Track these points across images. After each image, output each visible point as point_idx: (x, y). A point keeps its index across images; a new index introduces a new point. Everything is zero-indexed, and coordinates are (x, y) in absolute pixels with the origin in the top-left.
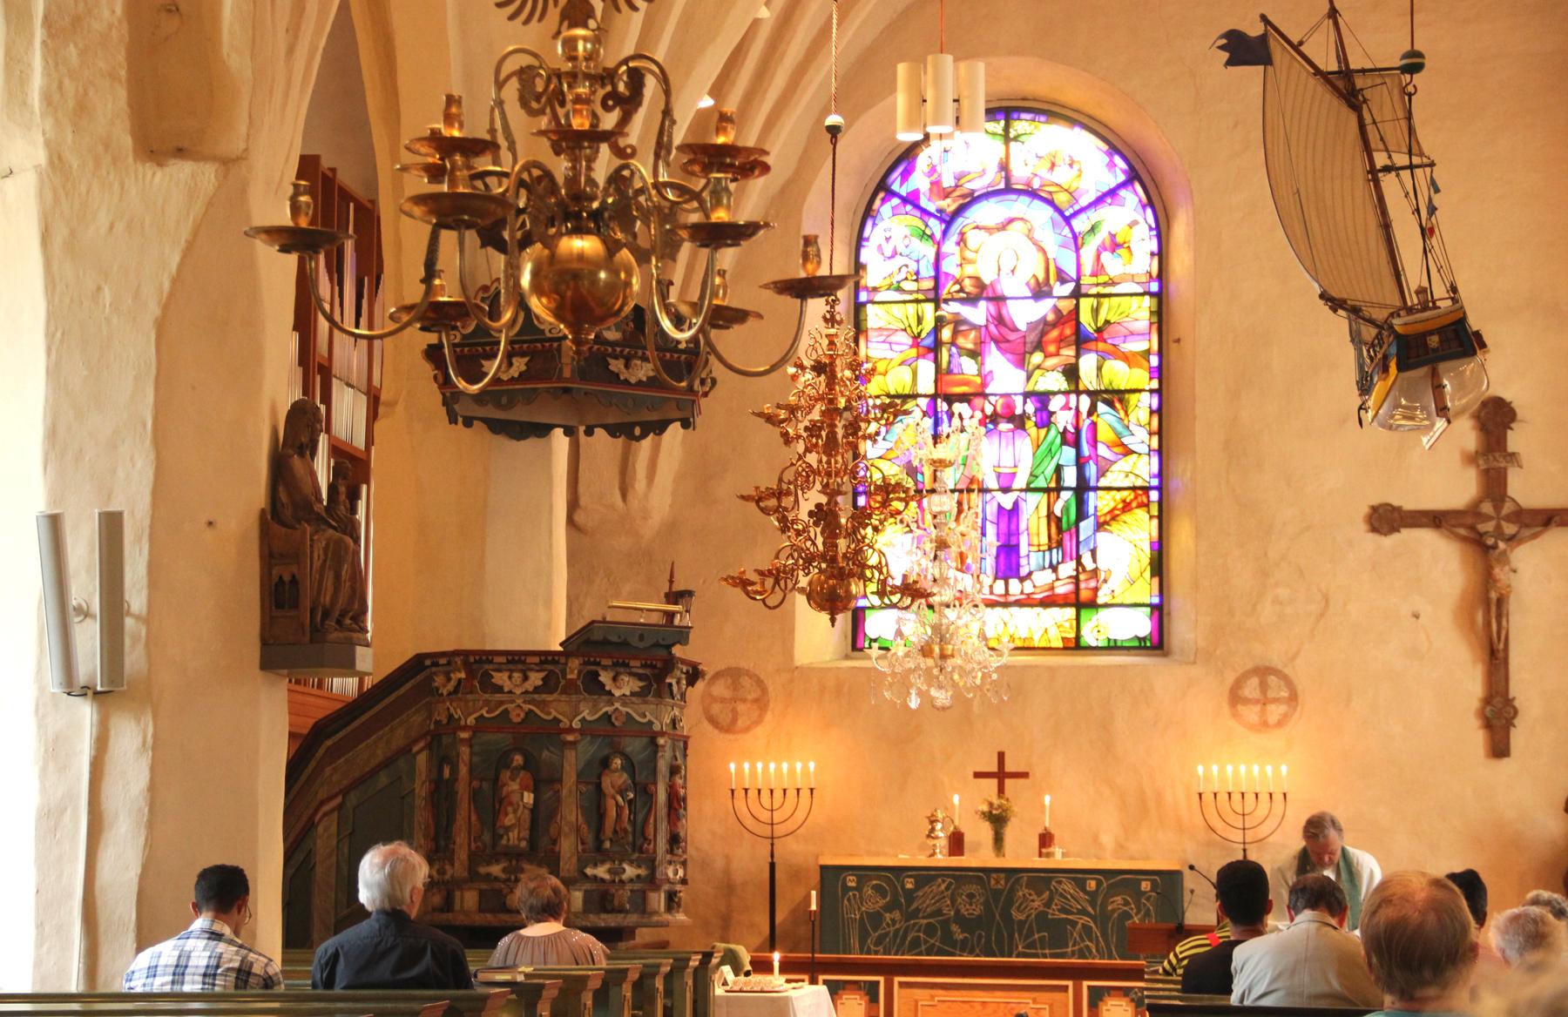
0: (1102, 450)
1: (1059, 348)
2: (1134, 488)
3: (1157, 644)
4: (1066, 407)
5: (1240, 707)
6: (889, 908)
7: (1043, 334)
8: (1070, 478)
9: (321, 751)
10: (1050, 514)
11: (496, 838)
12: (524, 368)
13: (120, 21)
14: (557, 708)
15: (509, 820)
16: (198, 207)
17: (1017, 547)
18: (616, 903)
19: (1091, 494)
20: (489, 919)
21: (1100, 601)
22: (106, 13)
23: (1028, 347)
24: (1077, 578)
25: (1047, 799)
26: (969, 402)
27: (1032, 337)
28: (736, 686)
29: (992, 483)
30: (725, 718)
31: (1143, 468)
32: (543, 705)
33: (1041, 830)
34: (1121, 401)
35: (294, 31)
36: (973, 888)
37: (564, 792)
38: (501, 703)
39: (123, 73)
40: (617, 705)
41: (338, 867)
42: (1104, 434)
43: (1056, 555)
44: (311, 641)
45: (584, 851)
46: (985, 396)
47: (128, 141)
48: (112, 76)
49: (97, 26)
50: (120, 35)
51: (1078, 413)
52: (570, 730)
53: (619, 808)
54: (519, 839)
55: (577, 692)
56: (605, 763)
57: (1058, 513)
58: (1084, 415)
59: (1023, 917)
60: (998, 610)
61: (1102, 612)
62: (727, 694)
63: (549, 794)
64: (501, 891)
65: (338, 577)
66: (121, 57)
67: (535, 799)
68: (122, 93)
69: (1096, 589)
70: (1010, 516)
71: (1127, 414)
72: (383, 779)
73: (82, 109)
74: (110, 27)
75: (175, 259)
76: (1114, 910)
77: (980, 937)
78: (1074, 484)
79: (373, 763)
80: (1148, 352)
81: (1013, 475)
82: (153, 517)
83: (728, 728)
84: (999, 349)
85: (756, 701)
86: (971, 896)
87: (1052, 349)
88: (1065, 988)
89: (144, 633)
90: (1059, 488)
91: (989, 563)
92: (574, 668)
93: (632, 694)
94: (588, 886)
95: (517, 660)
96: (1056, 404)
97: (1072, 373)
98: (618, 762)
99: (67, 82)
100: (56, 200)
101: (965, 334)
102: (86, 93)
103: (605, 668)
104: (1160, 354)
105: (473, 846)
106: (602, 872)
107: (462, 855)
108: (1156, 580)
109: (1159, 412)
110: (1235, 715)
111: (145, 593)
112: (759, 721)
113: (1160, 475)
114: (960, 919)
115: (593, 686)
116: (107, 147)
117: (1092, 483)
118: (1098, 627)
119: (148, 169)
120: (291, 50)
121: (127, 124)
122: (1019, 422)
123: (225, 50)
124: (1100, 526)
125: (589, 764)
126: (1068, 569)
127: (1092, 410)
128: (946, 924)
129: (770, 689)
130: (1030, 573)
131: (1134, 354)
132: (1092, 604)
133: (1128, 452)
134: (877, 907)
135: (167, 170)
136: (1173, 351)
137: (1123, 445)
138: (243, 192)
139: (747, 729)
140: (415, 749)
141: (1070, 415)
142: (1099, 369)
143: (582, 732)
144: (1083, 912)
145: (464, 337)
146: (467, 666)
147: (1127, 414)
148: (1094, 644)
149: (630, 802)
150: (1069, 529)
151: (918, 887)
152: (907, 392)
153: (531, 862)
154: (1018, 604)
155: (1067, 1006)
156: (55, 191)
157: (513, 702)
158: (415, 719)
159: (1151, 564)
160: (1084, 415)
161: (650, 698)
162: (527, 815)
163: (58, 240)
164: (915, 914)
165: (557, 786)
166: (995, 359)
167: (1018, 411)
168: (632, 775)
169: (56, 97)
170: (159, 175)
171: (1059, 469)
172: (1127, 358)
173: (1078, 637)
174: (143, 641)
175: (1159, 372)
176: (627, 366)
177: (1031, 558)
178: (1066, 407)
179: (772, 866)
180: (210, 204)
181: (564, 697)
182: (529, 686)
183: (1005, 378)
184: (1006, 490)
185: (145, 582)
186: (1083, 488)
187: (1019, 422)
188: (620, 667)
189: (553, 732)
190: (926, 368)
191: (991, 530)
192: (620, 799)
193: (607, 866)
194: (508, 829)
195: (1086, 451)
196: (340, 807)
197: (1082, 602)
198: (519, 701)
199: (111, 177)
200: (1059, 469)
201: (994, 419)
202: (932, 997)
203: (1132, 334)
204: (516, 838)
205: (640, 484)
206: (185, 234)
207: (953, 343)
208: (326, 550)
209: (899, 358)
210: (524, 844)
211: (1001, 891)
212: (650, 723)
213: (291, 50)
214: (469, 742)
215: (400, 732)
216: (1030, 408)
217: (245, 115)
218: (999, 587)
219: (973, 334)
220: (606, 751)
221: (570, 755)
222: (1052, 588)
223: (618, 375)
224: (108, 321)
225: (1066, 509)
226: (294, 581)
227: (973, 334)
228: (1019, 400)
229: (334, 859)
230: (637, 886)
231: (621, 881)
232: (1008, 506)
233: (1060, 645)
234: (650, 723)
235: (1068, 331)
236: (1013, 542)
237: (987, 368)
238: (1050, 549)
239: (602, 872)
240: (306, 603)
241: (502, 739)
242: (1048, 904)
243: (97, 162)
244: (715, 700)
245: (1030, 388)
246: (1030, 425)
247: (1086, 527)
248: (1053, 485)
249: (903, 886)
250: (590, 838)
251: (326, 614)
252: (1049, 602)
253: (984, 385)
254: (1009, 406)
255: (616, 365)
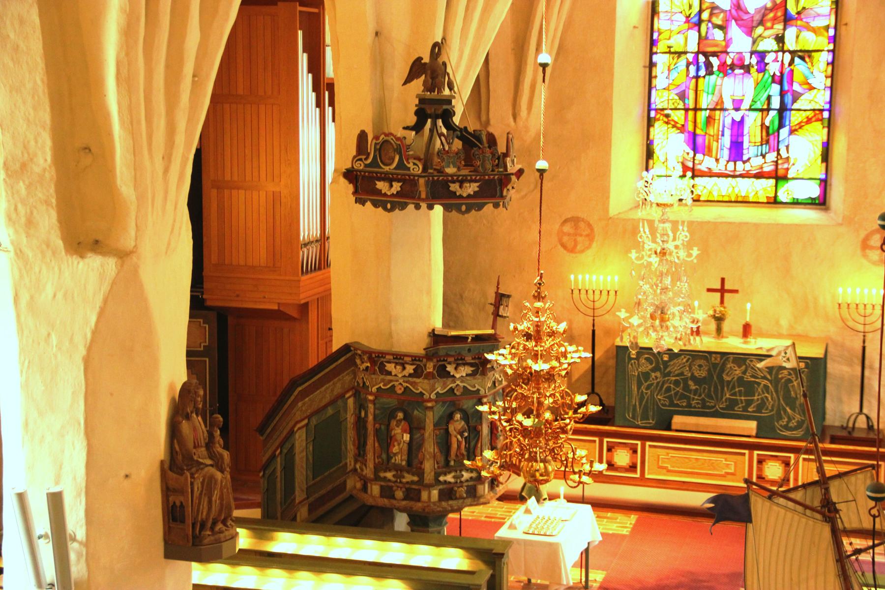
0: (796, 87)
1: (773, 24)
2: (814, 110)
3: (822, 202)
4: (776, 60)
5: (867, 251)
6: (654, 370)
7: (764, 15)
8: (776, 103)
9: (296, 393)
10: (763, 125)
11: (389, 458)
12: (399, 189)
13: (50, 167)
14: (422, 386)
15: (395, 449)
16: (106, 287)
17: (742, 143)
18: (458, 495)
19: (788, 112)
20: (385, 502)
21: (789, 176)
22: (41, 161)
23: (755, 24)
24: (776, 162)
25: (748, 306)
26: (718, 56)
27: (757, 17)
28: (576, 227)
29: (728, 104)
30: (570, 245)
31: (821, 98)
32: (412, 383)
33: (744, 322)
34: (809, 57)
35: (168, 158)
36: (702, 362)
37: (427, 435)
38: (391, 381)
39: (54, 201)
40: (458, 382)
41: (307, 459)
42: (797, 77)
43: (765, 148)
44: (193, 545)
45: (438, 467)
46: (727, 53)
47: (60, 243)
48: (47, 203)
49: (37, 170)
50: (50, 175)
51: (782, 64)
52: (430, 400)
53: (459, 443)
54: (402, 460)
55: (434, 377)
56: (450, 417)
57: (767, 124)
58: (786, 65)
59: (729, 379)
60: (730, 179)
61: (791, 182)
62: (572, 231)
63: (419, 435)
64: (392, 487)
65: (210, 502)
66: (52, 190)
67: (411, 438)
68: (54, 214)
69: (787, 169)
70: (738, 126)
71: (812, 65)
72: (330, 411)
73: (30, 223)
74: (44, 170)
75: (93, 319)
76: (782, 378)
77: (705, 388)
78: (778, 107)
79: (324, 402)
80: (827, 28)
81: (742, 101)
82: (87, 481)
83: (572, 250)
84: (737, 24)
85: (588, 235)
86: (700, 366)
87: (769, 24)
88: (744, 454)
89: (84, 553)
90: (769, 109)
91: (726, 154)
92: (430, 367)
93: (467, 375)
94: (441, 487)
95: (399, 359)
96: (769, 58)
97: (780, 39)
98: (458, 416)
99: (20, 206)
100: (21, 276)
101: (717, 15)
102: (32, 213)
103: (450, 363)
104: (836, 28)
105: (377, 461)
106: (449, 478)
107: (371, 465)
108: (824, 164)
109: (832, 63)
110: (865, 256)
111: (84, 528)
112: (589, 247)
113: (830, 103)
114: (693, 378)
115: (443, 373)
116: (48, 246)
117: (789, 107)
118: (786, 192)
119: (75, 259)
120: (166, 170)
121: (58, 233)
122: (747, 69)
123: (119, 182)
124: (792, 132)
125: (441, 418)
126: (772, 156)
127: (792, 62)
128: (685, 381)
129: (595, 230)
130: (749, 159)
131: (819, 28)
132: (785, 178)
133: (812, 88)
134: (647, 369)
135: (86, 260)
136: (843, 30)
137: (808, 84)
138: (135, 271)
139: (582, 251)
140: (347, 396)
141: (778, 64)
142: (797, 37)
143: (436, 401)
144: (764, 378)
145: (366, 166)
146: (370, 359)
147: (812, 65)
148: (784, 201)
149: (466, 438)
150: (773, 134)
151: (671, 359)
152: (681, 50)
153: (408, 472)
154: (742, 176)
155: (744, 463)
156: (20, 270)
157: (397, 381)
158: (346, 378)
159: (822, 155)
160: (786, 65)
161: (478, 376)
162: (406, 445)
163: (23, 302)
164: (669, 374)
165: (422, 431)
166: (735, 30)
167: (746, 63)
168: (467, 422)
169: (14, 216)
170: (81, 264)
171: (769, 98)
172: (814, 30)
173: (776, 197)
174: (84, 558)
175: (833, 40)
176: (461, 187)
177: (750, 149)
178: (776, 60)
179: (594, 331)
180: (114, 283)
181: (426, 381)
182: (406, 373)
183: (740, 43)
184: (737, 109)
185: (84, 521)
186: (783, 110)
187: (747, 69)
188: (460, 362)
189: (419, 400)
190: (693, 35)
191: (728, 133)
192: (459, 437)
193: (453, 474)
194: (395, 454)
195: (786, 88)
196: (307, 425)
197: (779, 176)
198: (401, 381)
199: (53, 262)
200: (769, 98)
201: (733, 67)
202: (668, 454)
203: (819, 15)
204: (400, 459)
205: (523, 113)
206: (99, 303)
207: (710, 21)
208: (202, 483)
209: (675, 27)
210: (404, 463)
211: (718, 364)
212: (478, 390)
213: (166, 170)
214: (373, 402)
215: (339, 385)
216: (754, 61)
217: (133, 224)
218: (731, 166)
219: (722, 15)
220: (452, 409)
221: (430, 414)
222: (762, 168)
223: (455, 193)
224: (56, 357)
225: (772, 122)
226: (182, 506)
227: (722, 15)
228: (747, 56)
229: (305, 453)
230: (470, 483)
231: (461, 482)
232: (738, 119)
233: (765, 201)
234: (478, 390)
235: (779, 14)
236: (740, 140)
237: (729, 36)
238: (762, 145)
239: (449, 478)
240: (189, 521)
241: (393, 402)
242: (744, 373)
243: (42, 252)
244: (564, 234)
245: (754, 49)
246: (753, 70)
247: (784, 132)
248: (765, 107)
249: (662, 359)
250: (442, 460)
251: (203, 526)
252: (760, 175)
253: (727, 46)
254: (741, 59)
255: (454, 187)
